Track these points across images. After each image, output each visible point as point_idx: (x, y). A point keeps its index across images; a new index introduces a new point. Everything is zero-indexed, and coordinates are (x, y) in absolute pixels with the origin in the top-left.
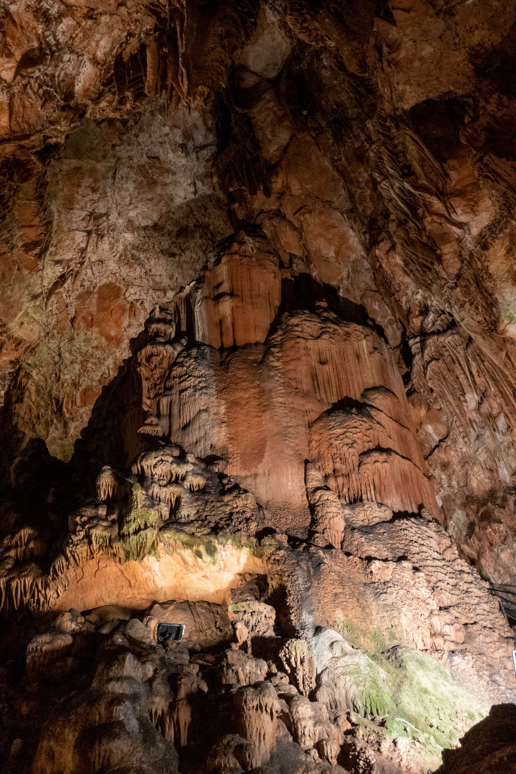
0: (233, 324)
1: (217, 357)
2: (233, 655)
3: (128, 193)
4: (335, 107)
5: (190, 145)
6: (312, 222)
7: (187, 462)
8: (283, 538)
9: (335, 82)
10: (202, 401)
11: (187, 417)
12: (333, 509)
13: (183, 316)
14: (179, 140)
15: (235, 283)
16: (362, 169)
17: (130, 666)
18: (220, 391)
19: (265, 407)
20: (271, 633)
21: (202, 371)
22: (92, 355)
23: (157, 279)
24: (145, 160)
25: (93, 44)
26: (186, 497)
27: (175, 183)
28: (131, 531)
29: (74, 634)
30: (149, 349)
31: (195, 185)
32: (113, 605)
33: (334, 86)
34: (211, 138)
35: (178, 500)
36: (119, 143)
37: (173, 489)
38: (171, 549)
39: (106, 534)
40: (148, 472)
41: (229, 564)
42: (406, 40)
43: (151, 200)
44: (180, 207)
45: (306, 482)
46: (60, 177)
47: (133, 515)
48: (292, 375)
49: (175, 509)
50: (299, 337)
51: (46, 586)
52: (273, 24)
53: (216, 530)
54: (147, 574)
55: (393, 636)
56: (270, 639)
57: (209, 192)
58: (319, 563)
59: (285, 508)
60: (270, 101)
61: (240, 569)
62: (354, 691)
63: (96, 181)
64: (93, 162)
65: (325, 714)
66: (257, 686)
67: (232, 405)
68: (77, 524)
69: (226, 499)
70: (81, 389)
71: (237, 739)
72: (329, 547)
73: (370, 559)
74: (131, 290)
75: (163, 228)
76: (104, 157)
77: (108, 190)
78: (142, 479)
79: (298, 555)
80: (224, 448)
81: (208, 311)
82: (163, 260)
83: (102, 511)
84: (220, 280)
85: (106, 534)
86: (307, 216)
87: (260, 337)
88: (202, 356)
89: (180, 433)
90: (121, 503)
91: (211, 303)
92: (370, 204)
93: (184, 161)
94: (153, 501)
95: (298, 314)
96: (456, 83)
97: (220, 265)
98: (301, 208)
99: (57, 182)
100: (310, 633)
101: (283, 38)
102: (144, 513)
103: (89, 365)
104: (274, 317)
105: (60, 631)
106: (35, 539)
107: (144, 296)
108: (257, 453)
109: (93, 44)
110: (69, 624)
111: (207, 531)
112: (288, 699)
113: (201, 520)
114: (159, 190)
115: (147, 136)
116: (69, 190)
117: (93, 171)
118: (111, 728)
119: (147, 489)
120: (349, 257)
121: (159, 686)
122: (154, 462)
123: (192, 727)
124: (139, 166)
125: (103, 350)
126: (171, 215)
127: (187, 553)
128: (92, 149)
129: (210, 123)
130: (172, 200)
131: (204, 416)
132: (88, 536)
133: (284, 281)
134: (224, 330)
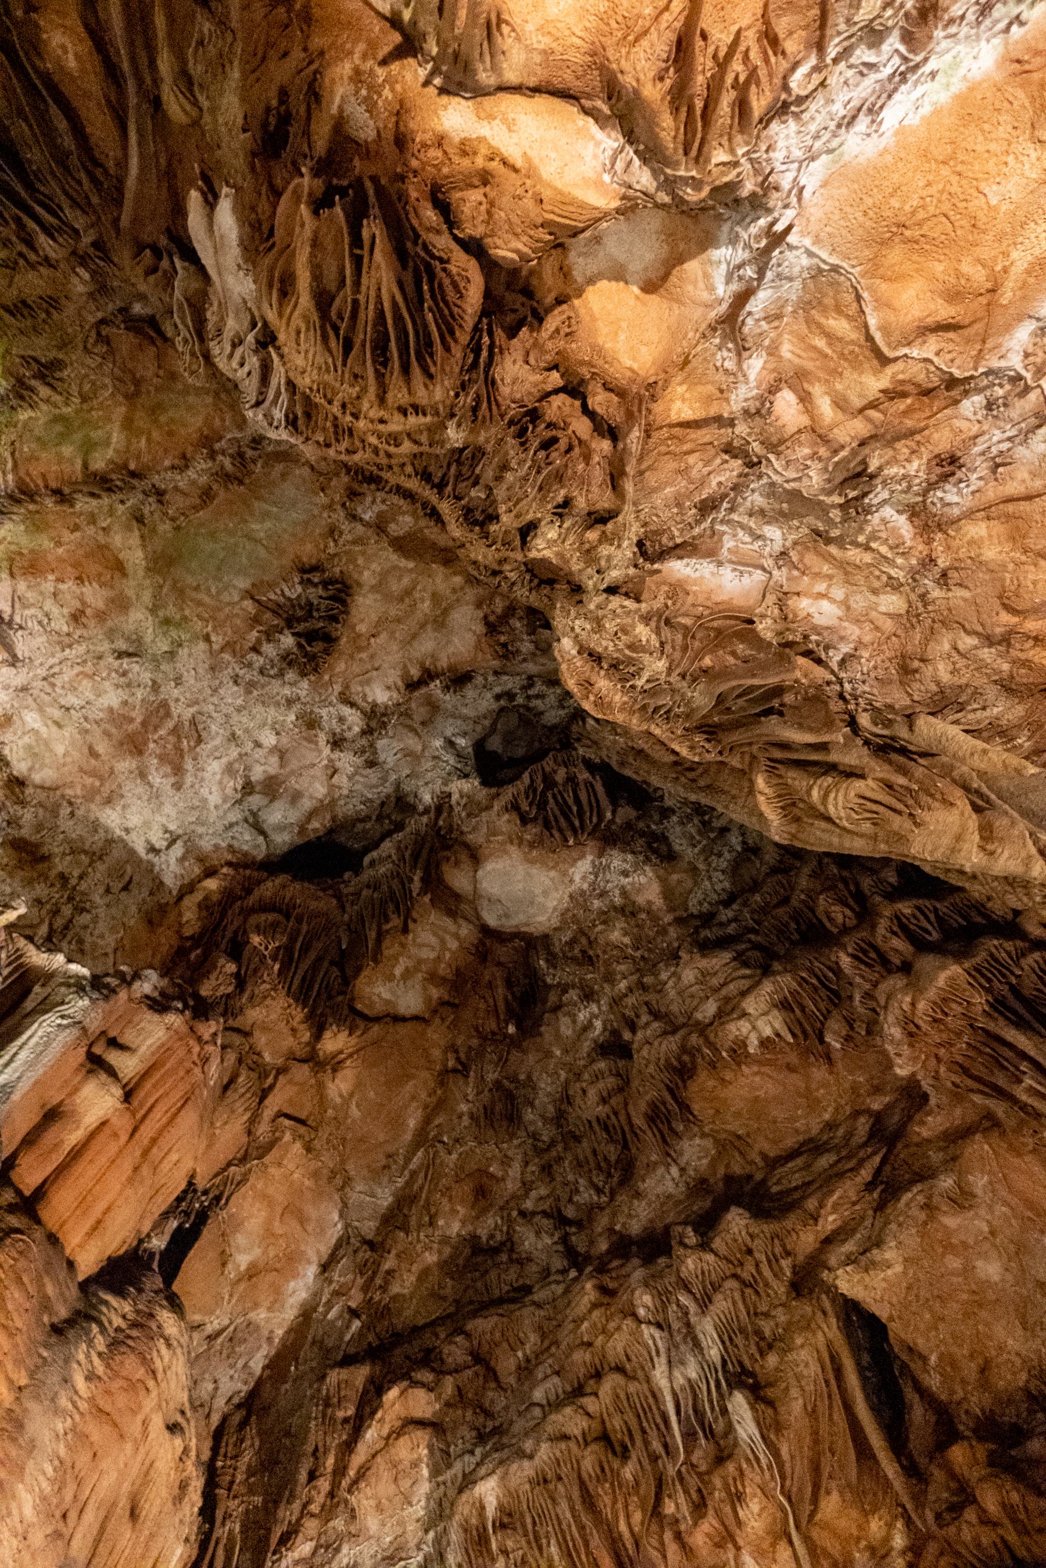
0: (76, 1154)
3: (92, 697)
4: (522, 1077)
5: (256, 800)
6: (290, 1165)
9: (558, 1053)
14: (258, 773)
15: (148, 1085)
16: (462, 1210)
24: (182, 712)
25: (821, 587)
27: (155, 796)
31: (172, 842)
33: (549, 1054)
34: (283, 840)
36: (216, 647)
42: (982, 1212)
43: (93, 753)
44: (95, 826)
46: (90, 531)
52: (571, 881)
57: (169, 880)
60: (457, 936)
63: (101, 616)
64: (147, 597)
75: (22, 803)
76: (167, 622)
77: (81, 649)
84: (128, 1037)
86: (297, 1147)
92: (410, 1279)
93: (214, 799)
96: (949, 1361)
97: (156, 1017)
98: (302, 1122)
99: (76, 528)
101: (555, 909)
104: (121, 1252)
109: (821, 587)
114: (125, 765)
115: (239, 702)
116: (61, 560)
117: (121, 604)
120: (256, 1305)
124: (164, 705)
126: (65, 811)
128: (180, 592)
129: (315, 824)
130: (108, 801)
134: (49, 1137)
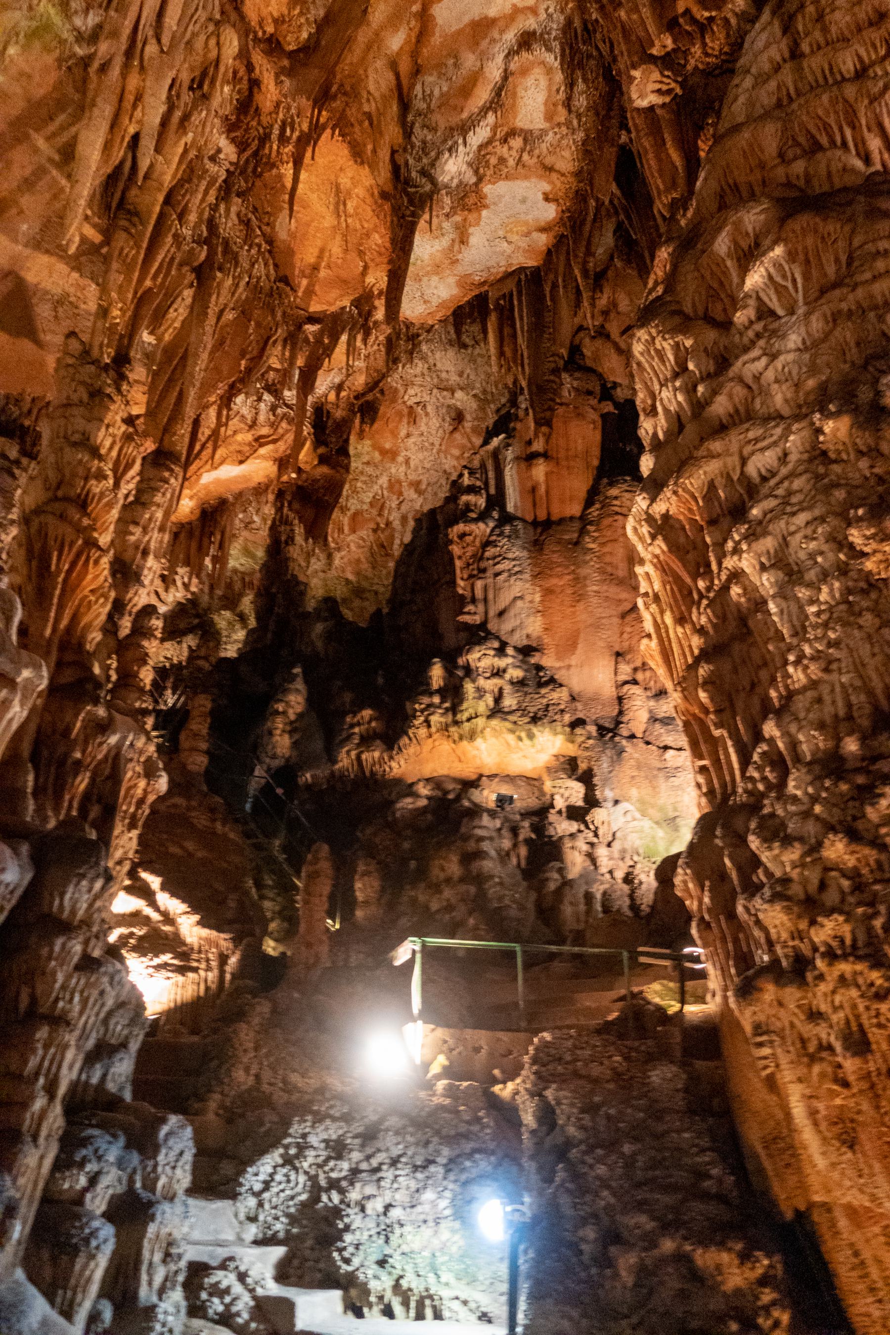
0: (547, 492)
1: (531, 534)
2: (552, 817)
7: (506, 655)
8: (592, 729)
10: (517, 587)
11: (501, 605)
12: (638, 703)
13: (492, 482)
17: (486, 820)
18: (534, 577)
19: (579, 597)
20: (580, 803)
21: (514, 552)
22: (362, 473)
23: (444, 375)
26: (507, 689)
28: (464, 718)
29: (429, 798)
30: (461, 527)
32: (447, 776)
35: (501, 690)
37: (496, 681)
38: (496, 733)
39: (443, 720)
40: (473, 665)
41: (547, 746)
45: (616, 674)
47: (465, 705)
48: (608, 559)
49: (498, 699)
50: (617, 513)
51: (391, 758)
53: (535, 720)
54: (475, 752)
55: (675, 810)
56: (580, 808)
58: (621, 752)
59: (595, 699)
61: (555, 751)
62: (638, 843)
65: (616, 855)
66: (572, 836)
67: (548, 592)
68: (415, 710)
69: (543, 691)
70: (349, 514)
71: (557, 864)
72: (633, 736)
73: (666, 748)
74: (411, 391)
78: (469, 671)
79: (605, 743)
80: (539, 638)
81: (518, 473)
82: (451, 353)
83: (436, 700)
85: (443, 720)
87: (575, 509)
88: (515, 534)
89: (496, 620)
90: (453, 693)
91: (523, 465)
94: (480, 693)
95: (617, 482)
100: (609, 804)
102: (475, 704)
103: (359, 484)
105: (417, 796)
106: (376, 719)
107: (427, 398)
108: (570, 645)
110: (424, 790)
111: (527, 720)
112: (592, 845)
113: (521, 710)
118: (479, 855)
119: (474, 681)
121: (505, 832)
122: (478, 655)
123: (528, 858)
125: (376, 466)
127: (511, 738)
131: (519, 603)
132: (428, 723)
133: (604, 417)
